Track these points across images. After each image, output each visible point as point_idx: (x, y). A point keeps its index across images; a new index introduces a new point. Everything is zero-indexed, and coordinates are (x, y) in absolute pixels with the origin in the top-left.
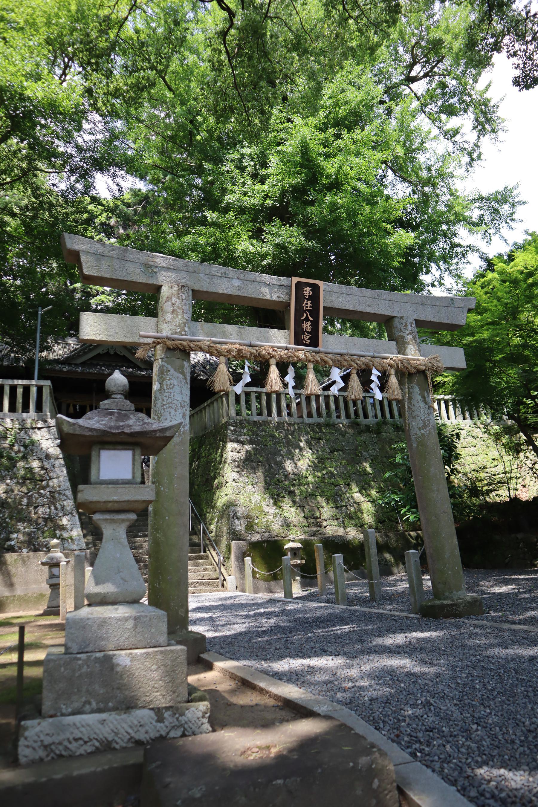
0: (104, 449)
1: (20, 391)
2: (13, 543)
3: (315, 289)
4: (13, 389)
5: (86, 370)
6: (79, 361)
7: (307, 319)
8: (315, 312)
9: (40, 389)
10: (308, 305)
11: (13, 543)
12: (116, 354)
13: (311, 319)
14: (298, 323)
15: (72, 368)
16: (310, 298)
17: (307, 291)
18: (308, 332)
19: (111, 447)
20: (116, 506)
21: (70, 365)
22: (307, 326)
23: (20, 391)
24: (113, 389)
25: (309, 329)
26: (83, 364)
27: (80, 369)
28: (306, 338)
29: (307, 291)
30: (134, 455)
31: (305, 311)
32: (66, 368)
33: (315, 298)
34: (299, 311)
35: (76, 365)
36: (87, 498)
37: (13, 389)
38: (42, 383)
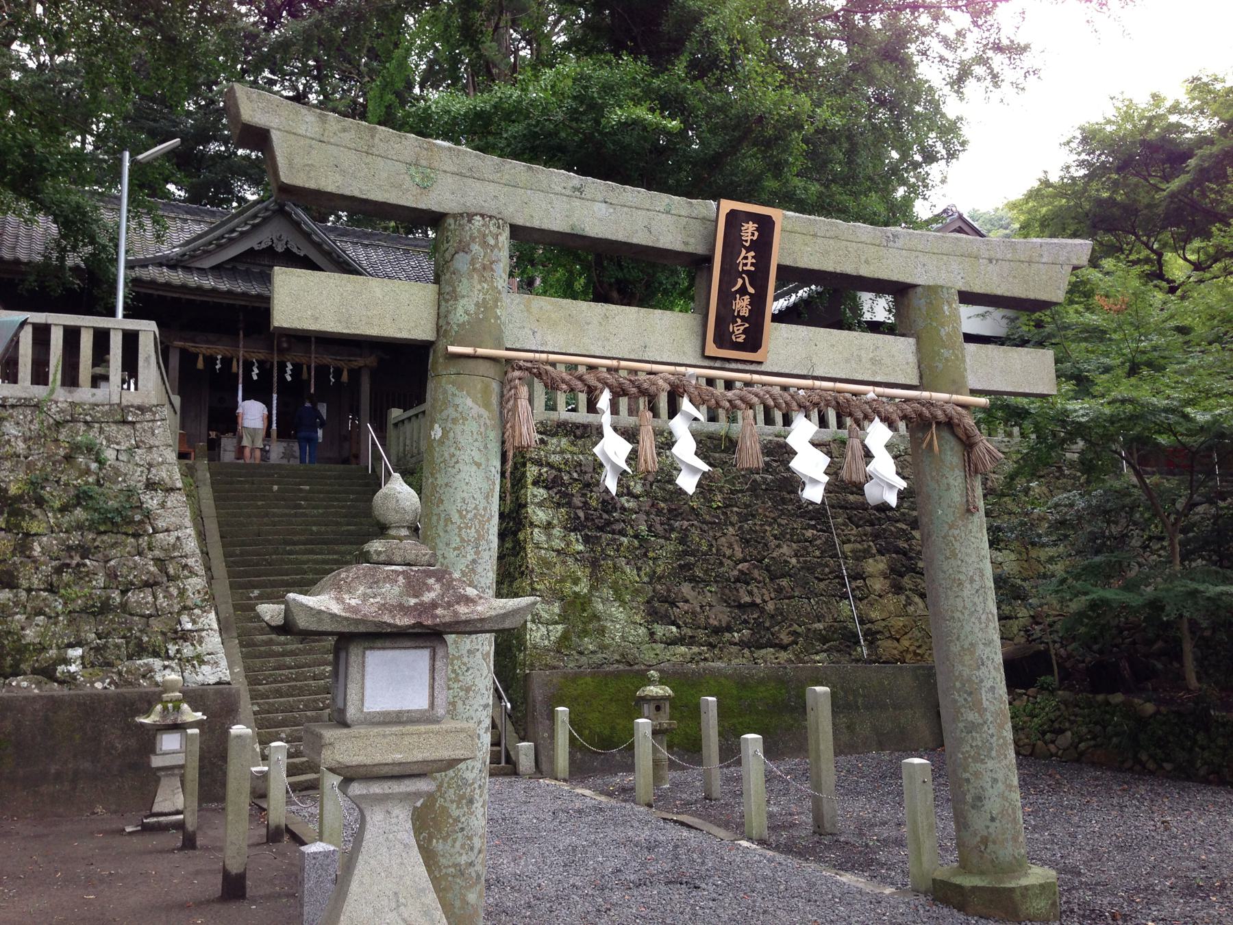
0: (372, 648)
1: (86, 343)
2: (73, 668)
3: (766, 224)
4: (72, 335)
5: (224, 286)
6: (208, 263)
7: (743, 291)
8: (759, 277)
9: (130, 339)
10: (747, 260)
11: (73, 668)
12: (288, 251)
13: (751, 290)
14: (726, 298)
15: (194, 280)
16: (754, 246)
17: (749, 231)
18: (743, 319)
19: (388, 644)
20: (396, 771)
21: (188, 269)
22: (742, 305)
23: (86, 343)
24: (392, 517)
25: (745, 312)
26: (218, 270)
27: (209, 282)
28: (738, 331)
29: (749, 231)
30: (433, 659)
31: (740, 275)
32: (177, 277)
33: (763, 246)
34: (730, 272)
35: (202, 271)
36: (339, 758)
37: (72, 335)
38: (132, 324)
